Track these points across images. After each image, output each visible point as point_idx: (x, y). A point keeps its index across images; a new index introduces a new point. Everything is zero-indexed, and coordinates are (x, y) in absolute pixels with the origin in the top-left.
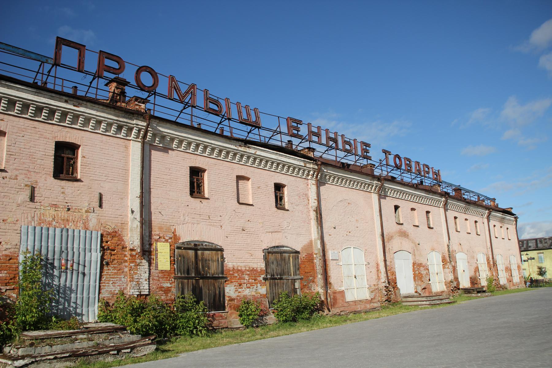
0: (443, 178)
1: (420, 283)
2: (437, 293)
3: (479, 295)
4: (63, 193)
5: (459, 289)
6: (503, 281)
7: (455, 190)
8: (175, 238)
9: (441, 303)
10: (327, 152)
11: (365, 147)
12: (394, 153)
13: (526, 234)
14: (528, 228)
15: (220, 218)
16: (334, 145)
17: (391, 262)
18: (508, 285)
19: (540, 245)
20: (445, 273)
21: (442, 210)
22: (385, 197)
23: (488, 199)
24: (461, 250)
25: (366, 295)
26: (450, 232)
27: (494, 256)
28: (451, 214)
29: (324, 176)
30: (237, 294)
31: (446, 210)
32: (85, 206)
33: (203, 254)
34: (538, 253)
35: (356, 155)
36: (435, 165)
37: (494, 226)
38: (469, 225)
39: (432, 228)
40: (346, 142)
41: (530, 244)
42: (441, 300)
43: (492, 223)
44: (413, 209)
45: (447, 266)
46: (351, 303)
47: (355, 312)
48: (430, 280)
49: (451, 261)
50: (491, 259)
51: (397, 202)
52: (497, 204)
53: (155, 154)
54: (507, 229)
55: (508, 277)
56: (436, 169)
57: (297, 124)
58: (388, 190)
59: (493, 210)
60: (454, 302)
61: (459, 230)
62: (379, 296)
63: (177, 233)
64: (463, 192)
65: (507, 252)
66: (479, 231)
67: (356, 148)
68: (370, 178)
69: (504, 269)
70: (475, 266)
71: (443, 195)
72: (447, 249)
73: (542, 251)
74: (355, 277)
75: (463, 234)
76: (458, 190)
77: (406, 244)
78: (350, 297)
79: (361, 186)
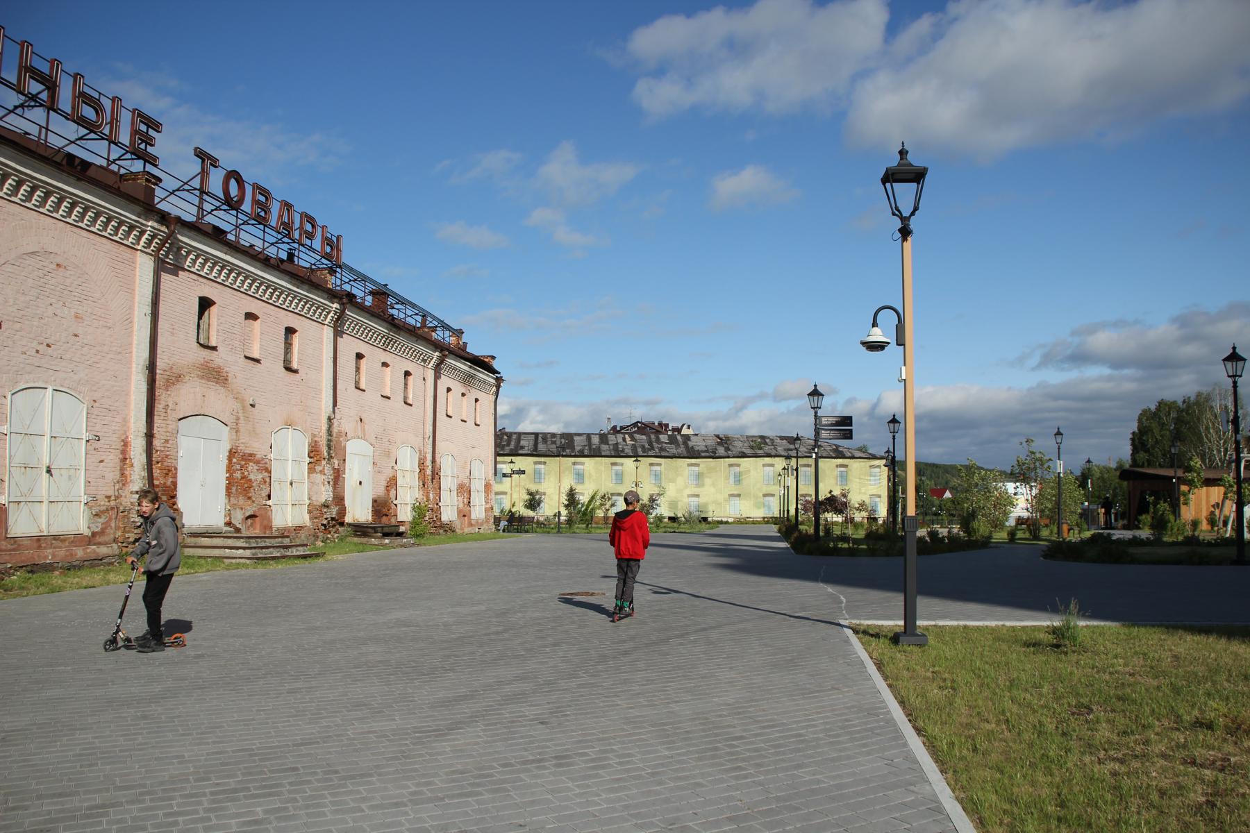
0: (346, 258)
1: (241, 501)
2: (285, 529)
3: (387, 541)
5: (342, 524)
6: (448, 514)
7: (372, 293)
9: (283, 557)
10: (19, 111)
11: (143, 128)
13: (527, 422)
14: (533, 412)
16: (44, 96)
17: (167, 441)
18: (457, 525)
19: (541, 447)
20: (312, 483)
21: (328, 333)
22: (176, 269)
23: (446, 327)
24: (360, 435)
25: (78, 521)
26: (339, 387)
27: (437, 456)
28: (349, 346)
29: (176, 248)
31: (338, 333)
34: (536, 463)
35: (112, 141)
36: (331, 220)
37: (449, 390)
38: (391, 380)
39: (296, 371)
40: (83, 97)
41: (523, 443)
42: (286, 547)
43: (444, 382)
44: (251, 316)
45: (319, 468)
46: (26, 542)
47: (34, 568)
48: (269, 497)
49: (330, 457)
50: (429, 463)
51: (210, 291)
52: (465, 344)
53: (165, 277)
54: (477, 400)
55: (461, 505)
56: (333, 231)
57: (148, 126)
58: (189, 253)
59: (451, 352)
60: (317, 555)
61: (362, 386)
62: (117, 528)
64: (391, 300)
65: (467, 452)
66: (410, 396)
67: (114, 122)
68: (138, 209)
69: (454, 488)
70: (390, 473)
71: (335, 297)
72: (325, 427)
73: (543, 459)
74: (49, 471)
75: (372, 397)
76: (381, 294)
77: (217, 400)
79: (106, 225)
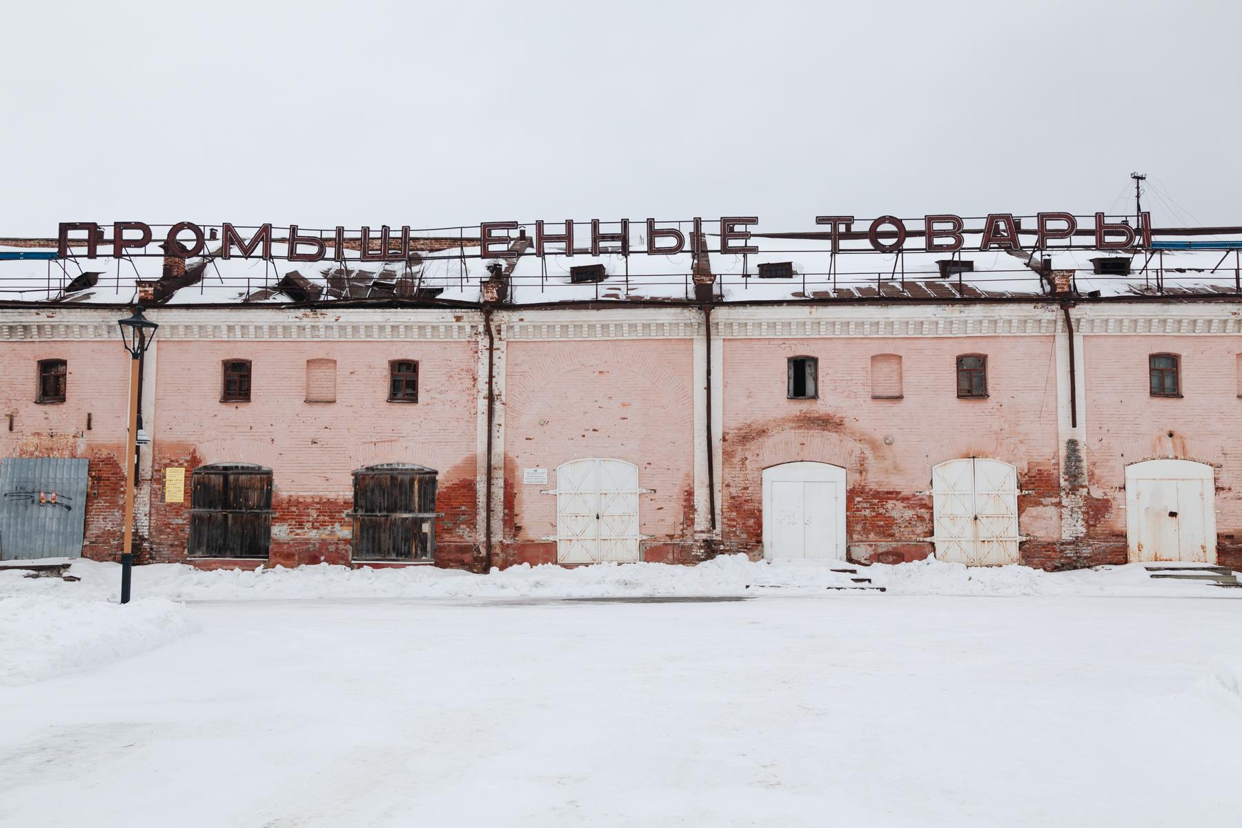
8: (194, 460)
15: (271, 429)
30: (292, 536)
32: (73, 431)
63: (198, 454)
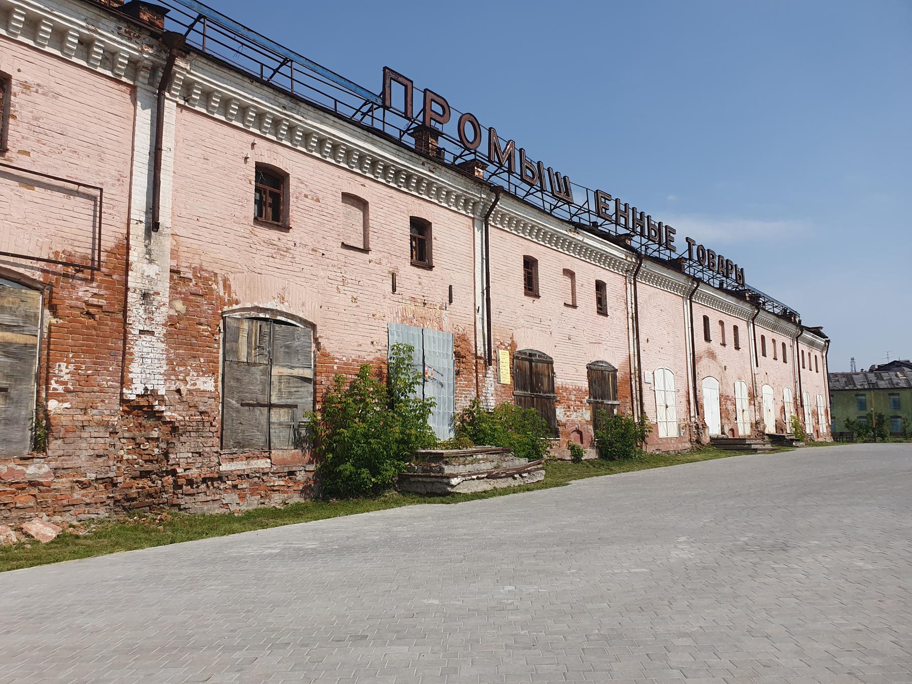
4: (420, 283)
8: (513, 345)
12: (698, 243)
25: (673, 433)
33: (536, 366)
78: (662, 434)
